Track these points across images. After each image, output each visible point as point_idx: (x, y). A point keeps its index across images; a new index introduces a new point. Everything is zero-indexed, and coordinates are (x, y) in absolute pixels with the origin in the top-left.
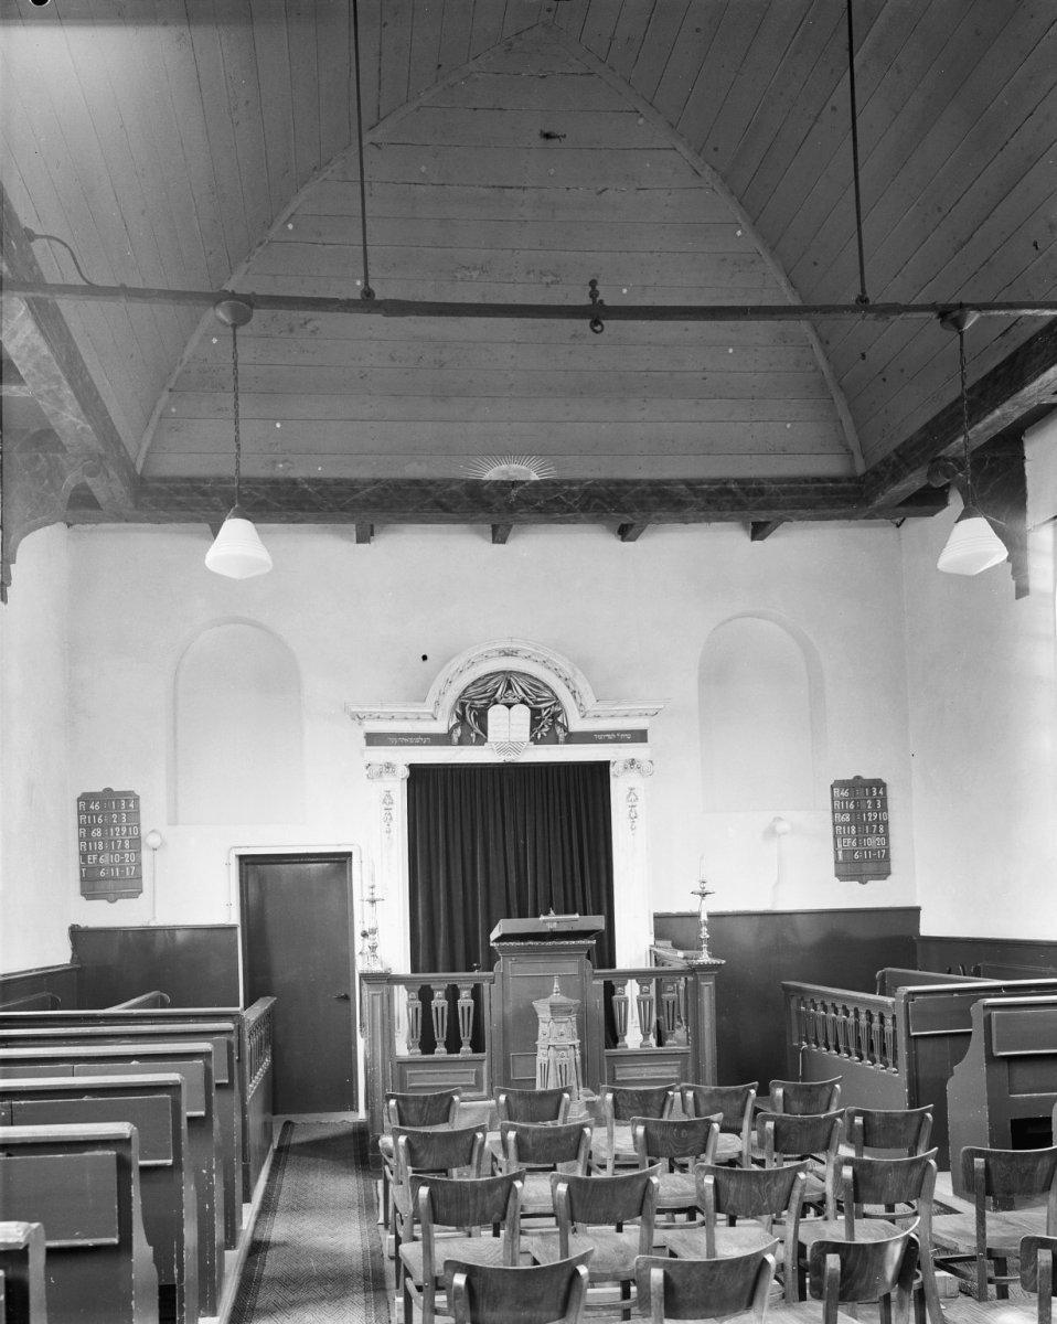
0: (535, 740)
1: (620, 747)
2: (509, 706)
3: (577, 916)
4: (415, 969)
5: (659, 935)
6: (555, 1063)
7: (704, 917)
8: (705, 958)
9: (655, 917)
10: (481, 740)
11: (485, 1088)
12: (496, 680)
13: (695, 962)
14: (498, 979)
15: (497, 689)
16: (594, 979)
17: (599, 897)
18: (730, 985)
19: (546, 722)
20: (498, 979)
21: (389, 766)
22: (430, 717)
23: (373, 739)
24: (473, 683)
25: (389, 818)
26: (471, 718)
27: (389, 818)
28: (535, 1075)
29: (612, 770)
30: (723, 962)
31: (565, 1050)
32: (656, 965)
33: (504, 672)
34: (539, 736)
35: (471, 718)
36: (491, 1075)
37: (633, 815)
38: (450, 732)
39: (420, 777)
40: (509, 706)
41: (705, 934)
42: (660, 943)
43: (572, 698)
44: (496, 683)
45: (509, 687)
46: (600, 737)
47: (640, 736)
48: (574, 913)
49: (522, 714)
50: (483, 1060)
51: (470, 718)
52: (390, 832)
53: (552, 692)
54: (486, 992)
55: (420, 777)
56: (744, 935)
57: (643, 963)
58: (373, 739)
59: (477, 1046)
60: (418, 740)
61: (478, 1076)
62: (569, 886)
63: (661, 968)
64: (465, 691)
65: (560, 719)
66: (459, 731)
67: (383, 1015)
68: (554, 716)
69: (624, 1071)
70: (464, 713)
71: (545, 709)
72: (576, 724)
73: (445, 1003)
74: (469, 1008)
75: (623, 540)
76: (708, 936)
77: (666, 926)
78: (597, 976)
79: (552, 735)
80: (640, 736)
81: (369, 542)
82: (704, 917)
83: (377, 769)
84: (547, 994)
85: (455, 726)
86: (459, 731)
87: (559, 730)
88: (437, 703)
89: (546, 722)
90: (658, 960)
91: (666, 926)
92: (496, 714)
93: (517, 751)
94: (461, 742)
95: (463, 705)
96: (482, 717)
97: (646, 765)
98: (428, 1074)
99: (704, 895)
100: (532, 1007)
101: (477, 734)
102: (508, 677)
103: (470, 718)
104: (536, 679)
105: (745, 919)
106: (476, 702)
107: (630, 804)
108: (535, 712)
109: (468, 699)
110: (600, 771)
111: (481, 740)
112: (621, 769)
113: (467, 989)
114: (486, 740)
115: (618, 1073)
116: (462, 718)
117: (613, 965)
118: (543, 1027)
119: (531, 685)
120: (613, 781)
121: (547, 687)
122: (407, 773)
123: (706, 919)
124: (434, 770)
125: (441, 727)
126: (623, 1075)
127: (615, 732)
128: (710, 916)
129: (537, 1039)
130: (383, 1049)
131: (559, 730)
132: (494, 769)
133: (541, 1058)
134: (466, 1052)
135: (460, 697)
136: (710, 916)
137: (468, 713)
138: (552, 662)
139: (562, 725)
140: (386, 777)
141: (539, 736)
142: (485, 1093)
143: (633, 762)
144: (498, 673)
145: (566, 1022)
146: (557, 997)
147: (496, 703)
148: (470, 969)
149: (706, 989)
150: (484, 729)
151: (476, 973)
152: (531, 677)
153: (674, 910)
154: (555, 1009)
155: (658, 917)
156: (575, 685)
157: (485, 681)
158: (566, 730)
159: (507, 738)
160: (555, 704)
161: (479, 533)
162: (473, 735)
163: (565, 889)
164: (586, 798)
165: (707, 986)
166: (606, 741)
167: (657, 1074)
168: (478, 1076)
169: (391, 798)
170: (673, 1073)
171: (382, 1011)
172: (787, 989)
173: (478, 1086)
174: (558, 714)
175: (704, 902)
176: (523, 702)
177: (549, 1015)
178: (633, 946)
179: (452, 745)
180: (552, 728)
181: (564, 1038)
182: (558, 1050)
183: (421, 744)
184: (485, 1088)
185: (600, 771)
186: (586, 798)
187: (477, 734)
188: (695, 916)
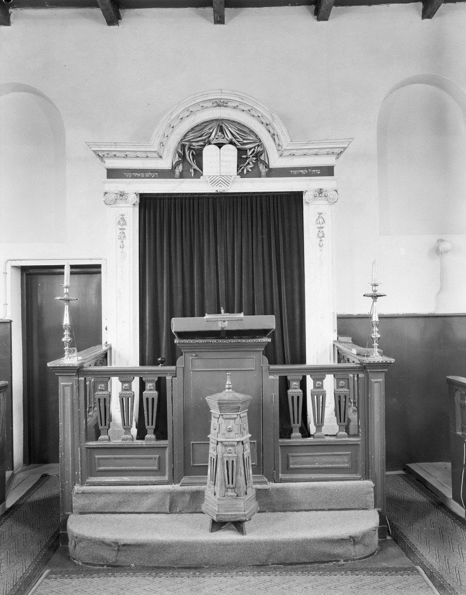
0: (241, 175)
1: (311, 180)
2: (220, 145)
3: (242, 315)
4: (142, 363)
5: (341, 332)
6: (222, 458)
7: (375, 318)
8: (376, 356)
9: (337, 318)
10: (198, 174)
11: (167, 473)
12: (209, 127)
13: (367, 360)
14: (180, 373)
15: (211, 133)
16: (270, 374)
17: (293, 301)
19: (251, 159)
20: (180, 373)
21: (122, 194)
22: (155, 155)
23: (112, 173)
24: (192, 129)
25: (122, 236)
26: (190, 158)
27: (122, 236)
28: (208, 463)
29: (305, 198)
30: (393, 360)
31: (234, 446)
32: (339, 362)
33: (217, 120)
34: (245, 172)
35: (190, 158)
36: (172, 461)
37: (321, 235)
38: (174, 167)
39: (147, 202)
40: (220, 145)
41: (376, 335)
42: (342, 339)
43: (272, 140)
44: (210, 129)
45: (222, 130)
46: (295, 172)
47: (328, 171)
48: (240, 312)
49: (231, 152)
50: (166, 447)
51: (189, 158)
52: (123, 247)
53: (256, 136)
54: (168, 385)
55: (147, 202)
56: (413, 332)
57: (328, 360)
58: (112, 173)
59: (161, 433)
60: (147, 175)
61: (161, 461)
62: (268, 292)
63: (342, 365)
64: (186, 135)
65: (262, 158)
66: (181, 167)
67: (72, 404)
68: (257, 155)
69: (298, 459)
70: (184, 153)
71: (250, 149)
72: (276, 162)
73: (155, 393)
74: (153, 399)
75: (318, 19)
76: (379, 336)
77: (347, 325)
78: (272, 372)
79: (256, 170)
80: (328, 171)
81: (118, 24)
82: (375, 318)
83: (113, 196)
84: (221, 389)
85: (178, 164)
86: (181, 167)
87: (261, 167)
88: (162, 144)
89: (251, 159)
90: (340, 357)
91: (347, 325)
92: (209, 152)
93: (227, 183)
94: (182, 176)
95: (183, 146)
96: (198, 156)
97: (332, 194)
98: (115, 458)
99: (375, 297)
100: (206, 401)
101: (195, 170)
102: (221, 125)
103: (189, 158)
104: (244, 126)
105: (413, 320)
106: (194, 144)
107: (319, 226)
108: (241, 152)
109: (188, 141)
110: (296, 199)
111: (198, 174)
112: (311, 197)
113: (151, 381)
114: (202, 175)
115: (291, 460)
116: (183, 157)
117: (303, 361)
118: (214, 422)
119: (239, 130)
120: (305, 208)
121: (252, 132)
122: (138, 200)
123: (377, 319)
124: (160, 199)
125: (166, 164)
126: (296, 463)
127: (307, 168)
128: (381, 317)
129: (209, 433)
130: (73, 436)
131: (261, 167)
132: (208, 198)
133: (212, 453)
134: (150, 439)
135: (181, 140)
136: (381, 317)
137: (187, 153)
138: (256, 110)
139: (263, 162)
140: (121, 204)
141: (245, 172)
142: (166, 478)
143: (321, 191)
144: (212, 121)
145: (235, 419)
146: (228, 395)
147: (210, 144)
148: (156, 363)
149: (376, 385)
150: (200, 166)
151: (160, 368)
152: (239, 123)
153: (355, 312)
154: (222, 405)
155: (340, 318)
156: (273, 129)
157: (202, 127)
158: (267, 166)
159: (219, 174)
160: (258, 146)
161: (204, 15)
162: (192, 171)
163: (265, 293)
164: (283, 221)
165: (378, 382)
166: (300, 175)
167: (328, 463)
168: (161, 461)
169: (124, 221)
170: (344, 463)
171: (72, 400)
172: (450, 382)
173: (160, 471)
174: (261, 153)
175: (375, 304)
176: (231, 143)
177: (218, 410)
178: (320, 342)
179: (174, 178)
180: (256, 164)
181: (232, 434)
182: (226, 446)
183: (150, 177)
184: (167, 473)
185: (296, 199)
186: (283, 221)
187: (195, 170)
188: (368, 317)
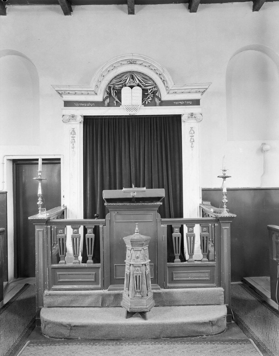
0: (145, 104)
1: (186, 108)
2: (132, 87)
3: (145, 189)
4: (85, 217)
5: (204, 199)
6: (133, 274)
7: (225, 190)
8: (225, 213)
9: (202, 190)
10: (118, 104)
11: (100, 283)
12: (125, 76)
13: (220, 215)
14: (108, 223)
15: (127, 80)
16: (162, 224)
17: (175, 180)
18: (237, 226)
19: (150, 95)
20: (108, 223)
21: (73, 116)
22: (93, 93)
23: (67, 104)
24: (115, 77)
25: (73, 141)
26: (114, 94)
27: (73, 141)
28: (124, 277)
29: (183, 118)
30: (235, 216)
31: (140, 267)
32: (203, 216)
33: (130, 72)
34: (147, 103)
35: (114, 94)
36: (103, 276)
37: (192, 140)
38: (104, 100)
39: (88, 121)
40: (132, 87)
41: (225, 200)
42: (205, 203)
43: (163, 84)
44: (126, 77)
45: (133, 78)
46: (177, 103)
47: (197, 102)
48: (144, 187)
49: (138, 91)
50: (99, 268)
51: (113, 94)
52: (74, 148)
53: (154, 81)
54: (101, 230)
55: (88, 121)
56: (247, 199)
57: (197, 216)
58: (67, 104)
59: (96, 259)
60: (88, 105)
61: (96, 276)
62: (160, 174)
63: (205, 218)
64: (111, 81)
65: (157, 94)
66: (108, 100)
67: (43, 242)
68: (154, 93)
69: (179, 275)
70: (110, 91)
71: (150, 89)
72: (165, 97)
73: (93, 235)
74: (92, 239)
75: (191, 12)
76: (227, 201)
77: (208, 195)
78: (163, 223)
79: (153, 102)
80: (197, 102)
81: (70, 14)
82: (225, 190)
83: (68, 117)
84: (132, 233)
85: (106, 98)
86: (108, 100)
87: (156, 100)
88: (97, 86)
89: (150, 95)
90: (204, 214)
91: (208, 195)
92: (125, 91)
93: (136, 109)
94: (109, 105)
95: (110, 87)
96: (119, 93)
97: (199, 116)
98: (69, 274)
99: (225, 178)
100: (123, 240)
101: (117, 102)
102: (132, 75)
103: (113, 94)
104: (146, 75)
105: (247, 191)
106: (116, 86)
107: (191, 135)
108: (144, 91)
109: (113, 84)
110: (177, 119)
111: (118, 104)
112: (186, 118)
113: (90, 228)
114: (121, 105)
115: (174, 275)
116: (110, 94)
117: (181, 216)
118: (128, 252)
119: (143, 78)
120: (183, 124)
121: (151, 79)
122: (82, 120)
123: (226, 191)
124: (96, 119)
125: (99, 98)
126: (177, 277)
127: (184, 101)
128: (228, 190)
129: (125, 259)
130: (44, 261)
131: (156, 100)
132: (125, 119)
133: (127, 271)
134: (90, 263)
135: (109, 84)
136: (228, 190)
137: (112, 92)
138: (153, 66)
139: (158, 97)
140: (73, 122)
141: (147, 103)
142: (100, 286)
143: (192, 114)
144: (127, 72)
145: (140, 250)
146: (136, 236)
147: (126, 86)
148: (93, 217)
149: (225, 231)
150: (120, 99)
151: (96, 220)
152: (143, 74)
153: (213, 187)
154: (133, 242)
155: (203, 190)
156: (164, 77)
157: (121, 76)
158: (160, 99)
159: (131, 104)
160: (155, 87)
161: (122, 9)
162: (115, 102)
163: (158, 176)
164: (169, 132)
165: (226, 229)
166: (180, 105)
167: (196, 277)
168: (96, 276)
169: (74, 132)
170: (206, 277)
171: (43, 239)
172: (270, 229)
173: (96, 282)
174: (156, 92)
175: (225, 182)
176: (138, 85)
177: (131, 246)
178: (192, 205)
179: (104, 106)
180: (153, 98)
181: (139, 260)
182: (135, 267)
183: (90, 106)
184: (100, 283)
185: (177, 119)
186: (169, 132)
187: (117, 102)
188: (220, 190)
